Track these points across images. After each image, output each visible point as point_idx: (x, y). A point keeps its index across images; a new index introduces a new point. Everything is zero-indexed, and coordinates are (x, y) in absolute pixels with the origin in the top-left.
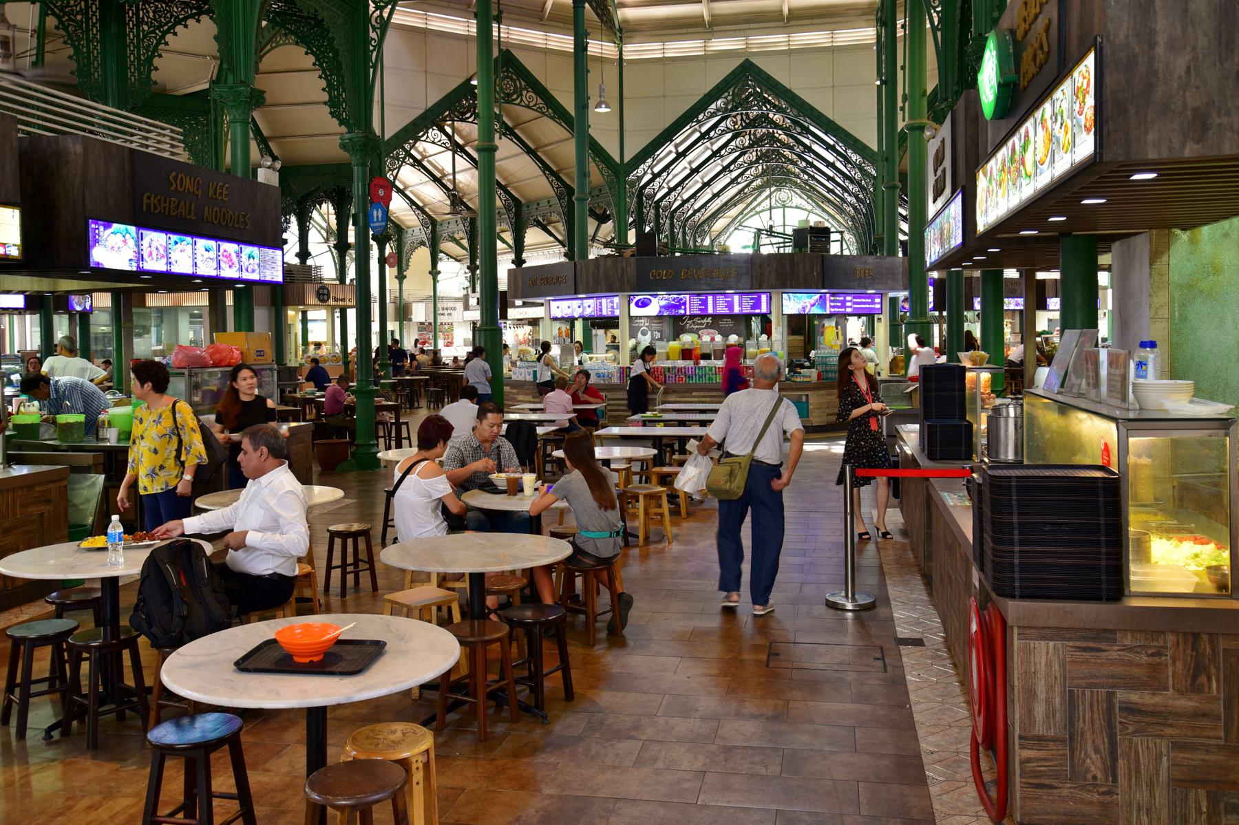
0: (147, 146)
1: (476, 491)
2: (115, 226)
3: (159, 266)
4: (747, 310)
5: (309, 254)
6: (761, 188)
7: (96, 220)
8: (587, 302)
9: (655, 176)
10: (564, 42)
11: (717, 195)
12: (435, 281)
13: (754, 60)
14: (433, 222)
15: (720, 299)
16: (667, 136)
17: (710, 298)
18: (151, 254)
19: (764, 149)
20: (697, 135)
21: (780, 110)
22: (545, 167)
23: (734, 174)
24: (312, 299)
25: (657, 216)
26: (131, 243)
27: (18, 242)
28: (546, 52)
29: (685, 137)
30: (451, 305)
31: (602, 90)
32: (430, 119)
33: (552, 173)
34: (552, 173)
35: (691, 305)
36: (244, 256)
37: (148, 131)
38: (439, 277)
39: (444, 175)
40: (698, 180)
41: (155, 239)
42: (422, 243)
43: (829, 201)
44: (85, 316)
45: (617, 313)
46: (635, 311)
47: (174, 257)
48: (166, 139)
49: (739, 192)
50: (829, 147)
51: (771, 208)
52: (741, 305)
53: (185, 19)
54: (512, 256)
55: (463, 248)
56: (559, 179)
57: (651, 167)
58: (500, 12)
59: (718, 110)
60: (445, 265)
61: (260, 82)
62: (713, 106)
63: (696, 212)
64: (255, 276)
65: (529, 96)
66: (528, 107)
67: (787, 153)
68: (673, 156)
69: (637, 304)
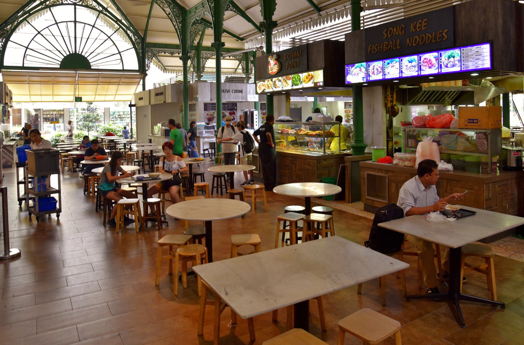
1: (56, 250)
2: (356, 65)
7: (348, 65)
18: (374, 73)
26: (364, 70)
27: (322, 80)
47: (387, 71)
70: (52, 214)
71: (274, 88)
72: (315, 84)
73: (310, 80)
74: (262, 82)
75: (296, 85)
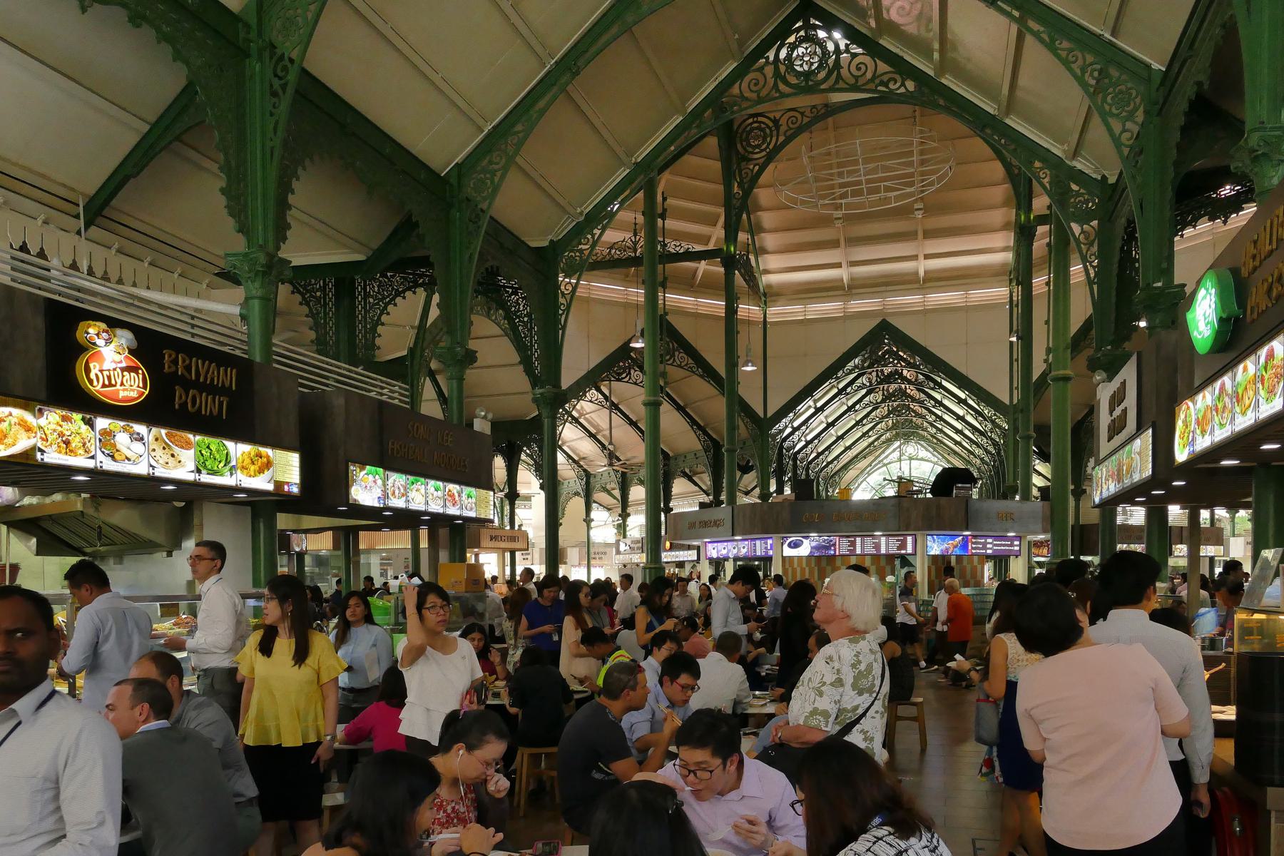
0: (394, 398)
3: (399, 503)
4: (893, 551)
5: (518, 495)
6: (889, 442)
7: (355, 462)
8: (741, 544)
9: (795, 430)
10: (716, 305)
11: (848, 448)
12: (589, 528)
13: (893, 321)
14: (588, 475)
15: (868, 540)
16: (808, 392)
17: (858, 540)
19: (895, 404)
20: (835, 391)
21: (910, 365)
22: (693, 422)
23: (866, 428)
24: (485, 542)
25: (795, 466)
26: (380, 482)
27: (298, 481)
28: (697, 316)
29: (823, 394)
30: (601, 550)
31: (748, 350)
32: (592, 379)
33: (700, 427)
34: (700, 427)
35: (841, 546)
36: (464, 496)
37: (382, 388)
38: (593, 524)
39: (599, 431)
40: (834, 432)
41: (397, 479)
42: (577, 494)
43: (955, 453)
44: (301, 556)
45: (771, 553)
46: (788, 552)
48: (396, 395)
49: (869, 446)
50: (961, 401)
51: (900, 460)
52: (887, 545)
53: (404, 292)
54: (619, 511)
55: (615, 498)
56: (705, 433)
57: (792, 421)
58: (665, 279)
59: (856, 367)
60: (598, 515)
61: (472, 345)
62: (851, 364)
63: (829, 463)
64: (472, 514)
65: (681, 356)
66: (680, 366)
67: (917, 408)
68: (812, 410)
69: (789, 545)
70: (786, 592)
71: (100, 456)
72: (279, 485)
73: (261, 471)
74: (28, 417)
75: (213, 472)
